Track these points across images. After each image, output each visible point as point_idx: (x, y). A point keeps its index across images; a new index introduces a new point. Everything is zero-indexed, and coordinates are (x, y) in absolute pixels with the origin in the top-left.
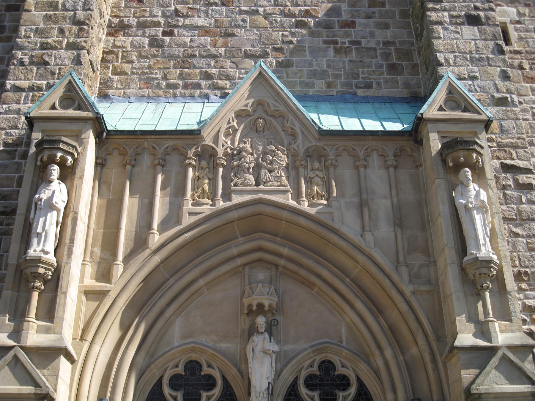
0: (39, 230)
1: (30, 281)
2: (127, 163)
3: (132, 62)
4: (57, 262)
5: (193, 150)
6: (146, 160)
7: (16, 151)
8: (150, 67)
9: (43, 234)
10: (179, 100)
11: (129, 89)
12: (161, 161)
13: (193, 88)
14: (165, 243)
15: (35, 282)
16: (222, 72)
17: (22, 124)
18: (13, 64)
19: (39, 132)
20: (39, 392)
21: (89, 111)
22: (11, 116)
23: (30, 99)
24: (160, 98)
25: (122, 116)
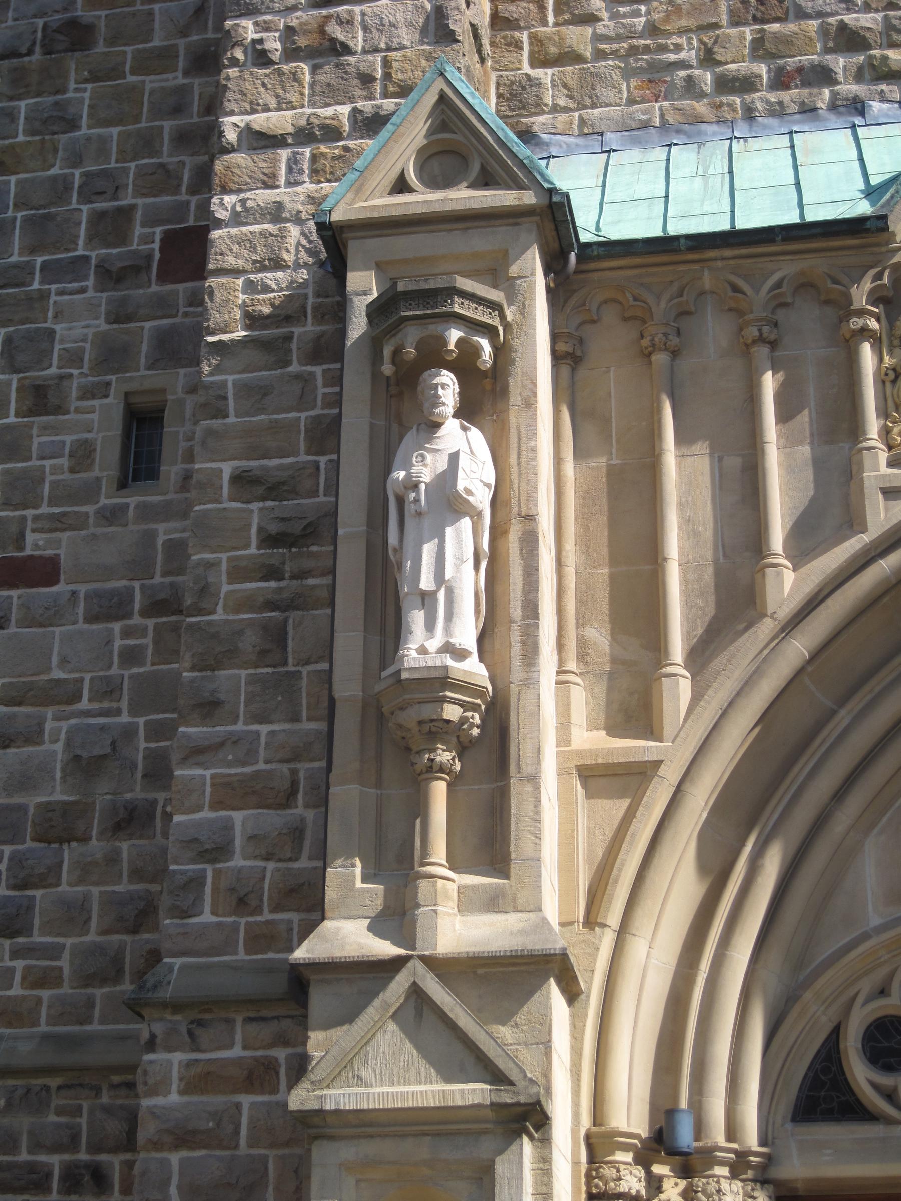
0: (426, 583)
1: (415, 748)
2: (653, 345)
3: (591, 19)
4: (492, 679)
5: (867, 285)
6: (714, 332)
7: (289, 338)
8: (653, 29)
9: (442, 596)
10: (765, 127)
11: (594, 106)
12: (766, 329)
13: (806, 83)
14: (818, 594)
15: (435, 750)
16: (896, 22)
17: (292, 250)
18: (234, 62)
19: (367, 268)
20: (507, 1099)
21: (520, 187)
22: (256, 228)
23: (306, 166)
24: (703, 126)
25: (625, 192)
